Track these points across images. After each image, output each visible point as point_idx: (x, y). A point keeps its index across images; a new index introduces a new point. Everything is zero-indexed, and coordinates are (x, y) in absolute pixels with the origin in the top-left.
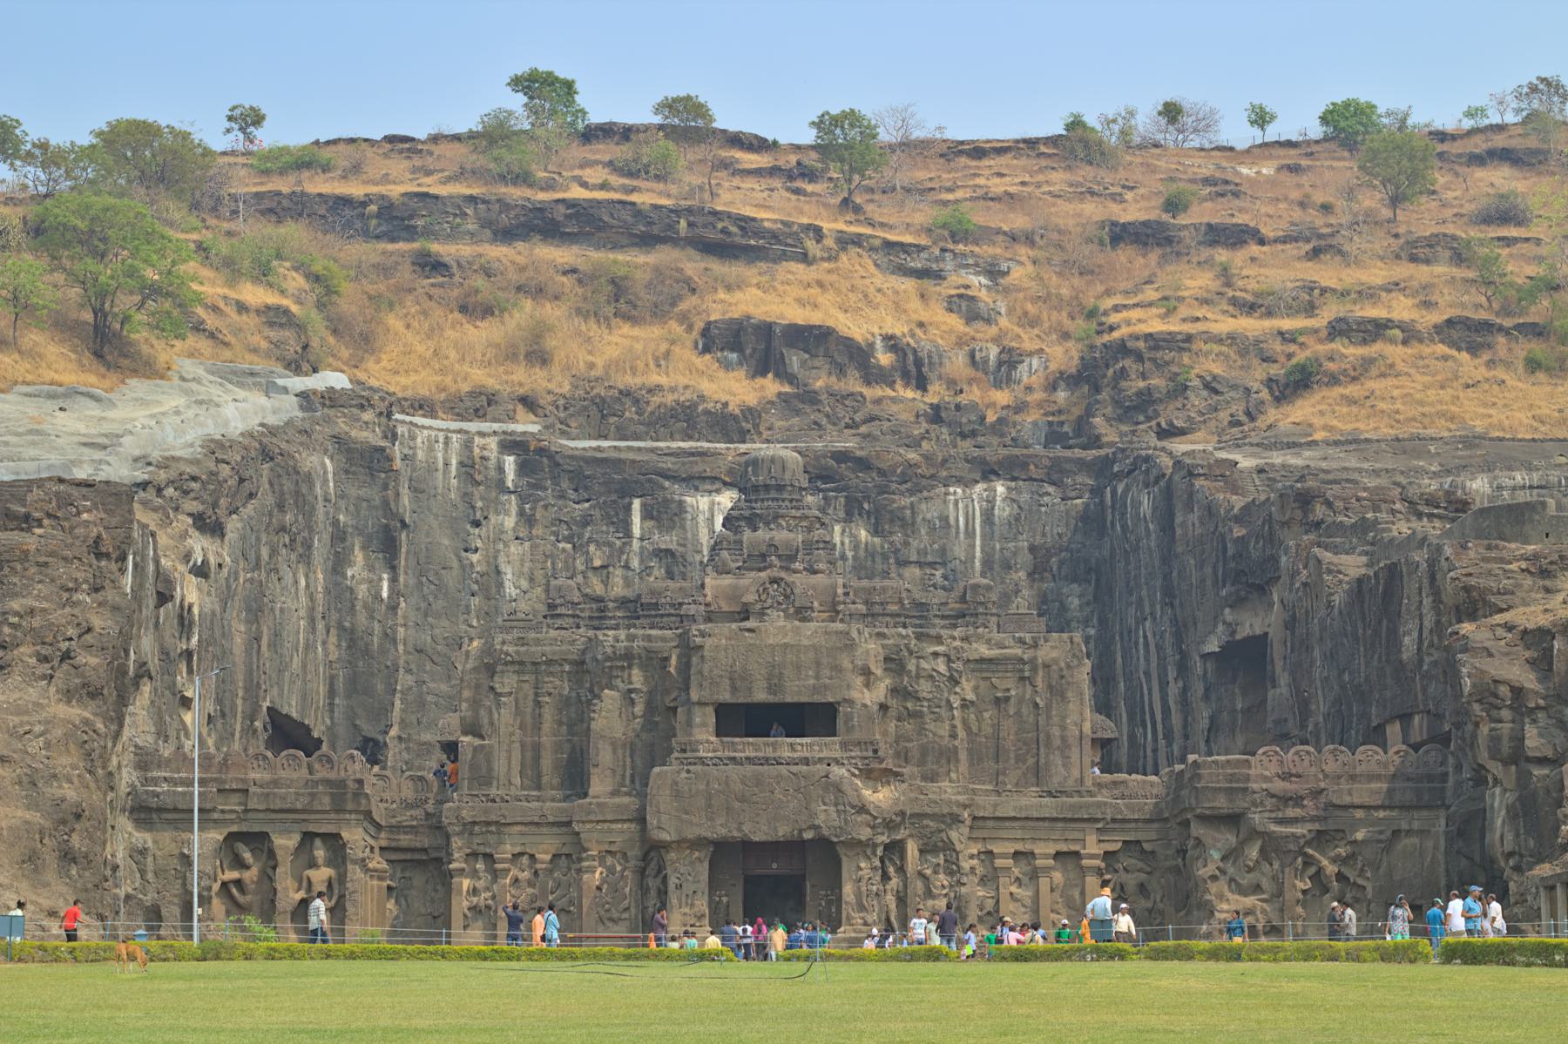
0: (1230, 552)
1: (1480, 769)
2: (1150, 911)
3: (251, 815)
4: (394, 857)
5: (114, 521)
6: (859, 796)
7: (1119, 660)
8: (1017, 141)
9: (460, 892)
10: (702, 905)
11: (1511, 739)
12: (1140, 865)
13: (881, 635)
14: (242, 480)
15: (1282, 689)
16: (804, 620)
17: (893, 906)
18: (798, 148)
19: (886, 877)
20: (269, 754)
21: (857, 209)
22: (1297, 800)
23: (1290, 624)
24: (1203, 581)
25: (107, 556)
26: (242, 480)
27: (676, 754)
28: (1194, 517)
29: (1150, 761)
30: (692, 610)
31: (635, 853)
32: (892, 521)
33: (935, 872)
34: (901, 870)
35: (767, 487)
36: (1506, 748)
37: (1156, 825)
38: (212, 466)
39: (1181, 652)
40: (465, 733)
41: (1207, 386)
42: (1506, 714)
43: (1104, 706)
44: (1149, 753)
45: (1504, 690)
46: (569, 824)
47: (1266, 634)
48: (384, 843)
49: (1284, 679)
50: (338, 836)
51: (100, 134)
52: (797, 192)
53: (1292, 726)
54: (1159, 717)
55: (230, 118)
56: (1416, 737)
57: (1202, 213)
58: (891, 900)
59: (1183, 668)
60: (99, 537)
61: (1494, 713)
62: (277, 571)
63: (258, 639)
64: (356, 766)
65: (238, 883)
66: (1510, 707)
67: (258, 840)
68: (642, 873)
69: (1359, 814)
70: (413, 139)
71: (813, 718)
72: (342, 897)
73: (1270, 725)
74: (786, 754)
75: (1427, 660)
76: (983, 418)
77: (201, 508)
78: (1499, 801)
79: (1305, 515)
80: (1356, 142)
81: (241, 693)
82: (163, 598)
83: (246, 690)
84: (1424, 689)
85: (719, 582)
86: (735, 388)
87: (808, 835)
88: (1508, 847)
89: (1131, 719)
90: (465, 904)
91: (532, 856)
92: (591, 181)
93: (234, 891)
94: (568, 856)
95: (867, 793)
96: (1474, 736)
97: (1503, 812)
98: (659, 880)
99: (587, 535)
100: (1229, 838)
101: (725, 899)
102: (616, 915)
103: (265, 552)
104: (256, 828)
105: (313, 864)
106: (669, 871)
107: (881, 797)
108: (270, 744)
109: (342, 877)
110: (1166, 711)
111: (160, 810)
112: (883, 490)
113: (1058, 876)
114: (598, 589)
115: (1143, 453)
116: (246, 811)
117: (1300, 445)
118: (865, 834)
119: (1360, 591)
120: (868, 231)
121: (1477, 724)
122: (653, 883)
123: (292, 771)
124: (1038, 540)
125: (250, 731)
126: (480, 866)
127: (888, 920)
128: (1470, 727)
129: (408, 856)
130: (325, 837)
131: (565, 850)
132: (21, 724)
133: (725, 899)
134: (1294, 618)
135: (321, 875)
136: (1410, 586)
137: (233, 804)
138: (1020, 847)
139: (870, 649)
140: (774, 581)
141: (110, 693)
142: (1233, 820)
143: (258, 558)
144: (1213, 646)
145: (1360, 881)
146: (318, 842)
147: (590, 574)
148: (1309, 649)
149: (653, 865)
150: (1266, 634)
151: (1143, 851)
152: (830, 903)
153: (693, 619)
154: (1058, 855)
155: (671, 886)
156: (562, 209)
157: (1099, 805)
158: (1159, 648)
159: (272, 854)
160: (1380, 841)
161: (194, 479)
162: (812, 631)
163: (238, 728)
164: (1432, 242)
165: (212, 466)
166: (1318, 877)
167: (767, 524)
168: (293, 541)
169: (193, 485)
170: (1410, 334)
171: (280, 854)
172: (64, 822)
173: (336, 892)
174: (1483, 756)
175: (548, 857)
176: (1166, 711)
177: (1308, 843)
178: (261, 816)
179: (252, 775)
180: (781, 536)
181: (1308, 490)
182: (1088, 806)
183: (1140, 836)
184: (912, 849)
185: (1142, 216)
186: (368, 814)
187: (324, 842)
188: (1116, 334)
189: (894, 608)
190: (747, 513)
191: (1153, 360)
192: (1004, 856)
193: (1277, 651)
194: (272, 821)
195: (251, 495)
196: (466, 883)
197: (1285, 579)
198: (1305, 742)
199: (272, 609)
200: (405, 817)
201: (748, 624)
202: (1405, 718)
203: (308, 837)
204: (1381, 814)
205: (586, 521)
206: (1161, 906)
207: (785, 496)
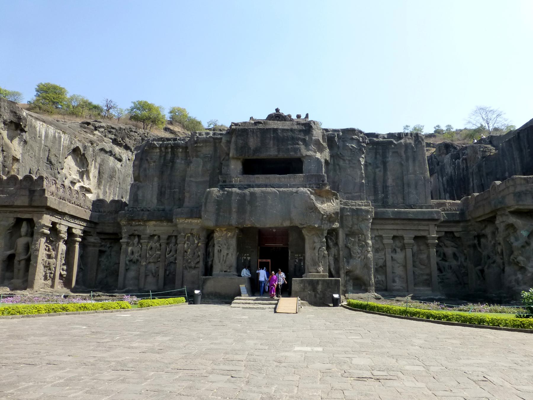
4: (103, 237)
12: (453, 244)
17: (332, 262)
19: (328, 248)
27: (221, 183)
33: (353, 245)
34: (336, 244)
91: (159, 237)
101: (249, 258)
102: (193, 264)
107: (329, 207)
133: (249, 258)
138: (395, 233)
151: (454, 237)
154: (416, 238)
161: (113, 128)
175: (166, 237)
183: (454, 229)
187: (27, 223)
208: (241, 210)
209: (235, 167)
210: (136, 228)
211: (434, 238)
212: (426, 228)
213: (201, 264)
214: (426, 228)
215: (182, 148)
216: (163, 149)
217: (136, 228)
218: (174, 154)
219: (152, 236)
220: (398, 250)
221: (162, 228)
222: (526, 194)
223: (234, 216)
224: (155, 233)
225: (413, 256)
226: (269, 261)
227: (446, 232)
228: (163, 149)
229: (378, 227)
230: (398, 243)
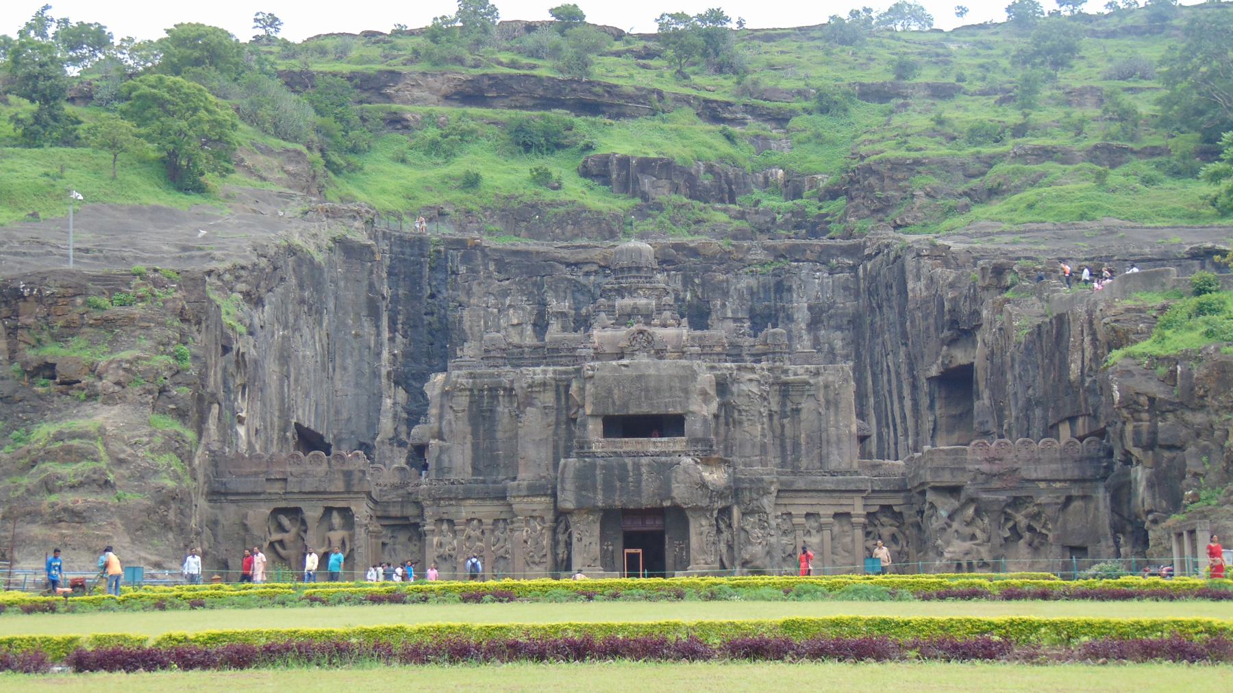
0: (946, 308)
1: (1127, 454)
2: (899, 553)
3: (288, 496)
5: (193, 298)
6: (701, 477)
7: (870, 383)
8: (794, 29)
9: (432, 545)
10: (596, 548)
11: (1149, 433)
12: (892, 522)
13: (712, 368)
14: (275, 269)
15: (983, 401)
16: (661, 358)
18: (642, 37)
19: (719, 531)
20: (301, 454)
21: (686, 77)
22: (1000, 475)
23: (991, 356)
24: (928, 328)
25: (188, 321)
26: (275, 269)
28: (922, 284)
29: (892, 452)
30: (584, 352)
31: (550, 516)
32: (714, 291)
34: (730, 526)
35: (630, 269)
36: (1145, 437)
37: (902, 494)
38: (255, 259)
39: (913, 377)
40: (434, 438)
41: (928, 195)
42: (1145, 416)
43: (861, 415)
44: (892, 445)
45: (1143, 399)
46: (504, 498)
47: (972, 364)
48: (379, 514)
49: (986, 394)
50: (348, 509)
51: (168, 31)
52: (644, 67)
53: (991, 426)
54: (898, 421)
55: (256, 20)
56: (1080, 431)
57: (929, 75)
58: (723, 547)
59: (914, 387)
60: (183, 308)
61: (1136, 415)
62: (299, 330)
63: (288, 377)
64: (358, 462)
65: (281, 542)
66: (1147, 411)
67: (294, 513)
68: (554, 531)
69: (1042, 485)
70: (381, 34)
71: (670, 425)
72: (352, 550)
73: (975, 425)
74: (652, 449)
75: (1088, 380)
76: (774, 219)
77: (248, 288)
78: (1140, 474)
79: (999, 281)
80: (539, 174)
81: (277, 414)
82: (226, 349)
83: (281, 411)
84: (1086, 400)
85: (603, 334)
86: (598, 200)
87: (667, 503)
88: (1147, 507)
89: (879, 423)
90: (436, 554)
91: (480, 521)
92: (503, 60)
93: (278, 547)
94: (505, 520)
95: (706, 474)
96: (1122, 431)
97: (1144, 483)
98: (566, 536)
99: (508, 302)
100: (954, 503)
101: (611, 548)
102: (537, 559)
103: (291, 320)
104: (292, 505)
105: (331, 529)
106: (572, 529)
108: (297, 447)
109: (352, 537)
110: (904, 418)
111: (226, 494)
112: (707, 270)
113: (836, 529)
114: (516, 339)
115: (886, 242)
116: (285, 493)
117: (993, 234)
118: (704, 503)
119: (1039, 334)
120: (694, 93)
121: (1124, 423)
122: (562, 538)
123: (316, 468)
124: (813, 302)
125: (283, 439)
126: (445, 527)
127: (721, 560)
128: (1119, 425)
129: (397, 522)
130: (340, 510)
131: (503, 516)
132: (133, 437)
133: (611, 548)
134: (992, 353)
135: (337, 536)
136: (1075, 329)
137: (277, 488)
139: (706, 378)
140: (641, 332)
141: (193, 415)
142: (954, 491)
143: (287, 323)
144: (934, 371)
145: (1044, 531)
146: (335, 514)
147: (510, 329)
148: (1003, 374)
149: (562, 525)
150: (972, 364)
151: (894, 512)
152: (682, 549)
153: (585, 358)
154: (836, 515)
155: (574, 540)
156: (487, 82)
157: (862, 481)
158: (898, 374)
159: (303, 522)
160: (1057, 504)
161: (243, 268)
162: (669, 366)
163: (275, 437)
164: (1082, 92)
165: (255, 259)
166: (1014, 529)
167: (630, 294)
168: (310, 309)
169: (243, 272)
170: (1065, 157)
171: (309, 522)
172: (163, 502)
173: (348, 547)
174: (1129, 445)
175: (491, 521)
176: (904, 418)
177: (1008, 505)
178: (296, 496)
179: (289, 469)
180: (642, 302)
181: (1001, 265)
182: (853, 482)
184: (736, 512)
185: (879, 80)
186: (369, 494)
188: (866, 161)
189: (719, 349)
190: (616, 286)
191: (892, 178)
192: (799, 516)
193: (980, 375)
194: (304, 500)
195: (282, 279)
196: (435, 540)
197: (985, 326)
198: (1001, 436)
199: (297, 357)
200: (392, 496)
201: (625, 362)
202: (1072, 420)
203: (328, 511)
204: (1058, 485)
205: (505, 293)
206: (906, 549)
207: (643, 274)
208: (608, 488)
209: (594, 429)
210: (444, 510)
211: (859, 516)
212: (850, 502)
213: (549, 557)
214: (850, 502)
215: (505, 389)
216: (476, 392)
217: (444, 510)
218: (494, 397)
219: (470, 521)
220: (813, 532)
221: (485, 509)
222: (943, 469)
223: (600, 497)
224: (473, 516)
225: (832, 539)
226: (640, 551)
227: (882, 507)
228: (476, 392)
229: (786, 501)
230: (813, 523)
